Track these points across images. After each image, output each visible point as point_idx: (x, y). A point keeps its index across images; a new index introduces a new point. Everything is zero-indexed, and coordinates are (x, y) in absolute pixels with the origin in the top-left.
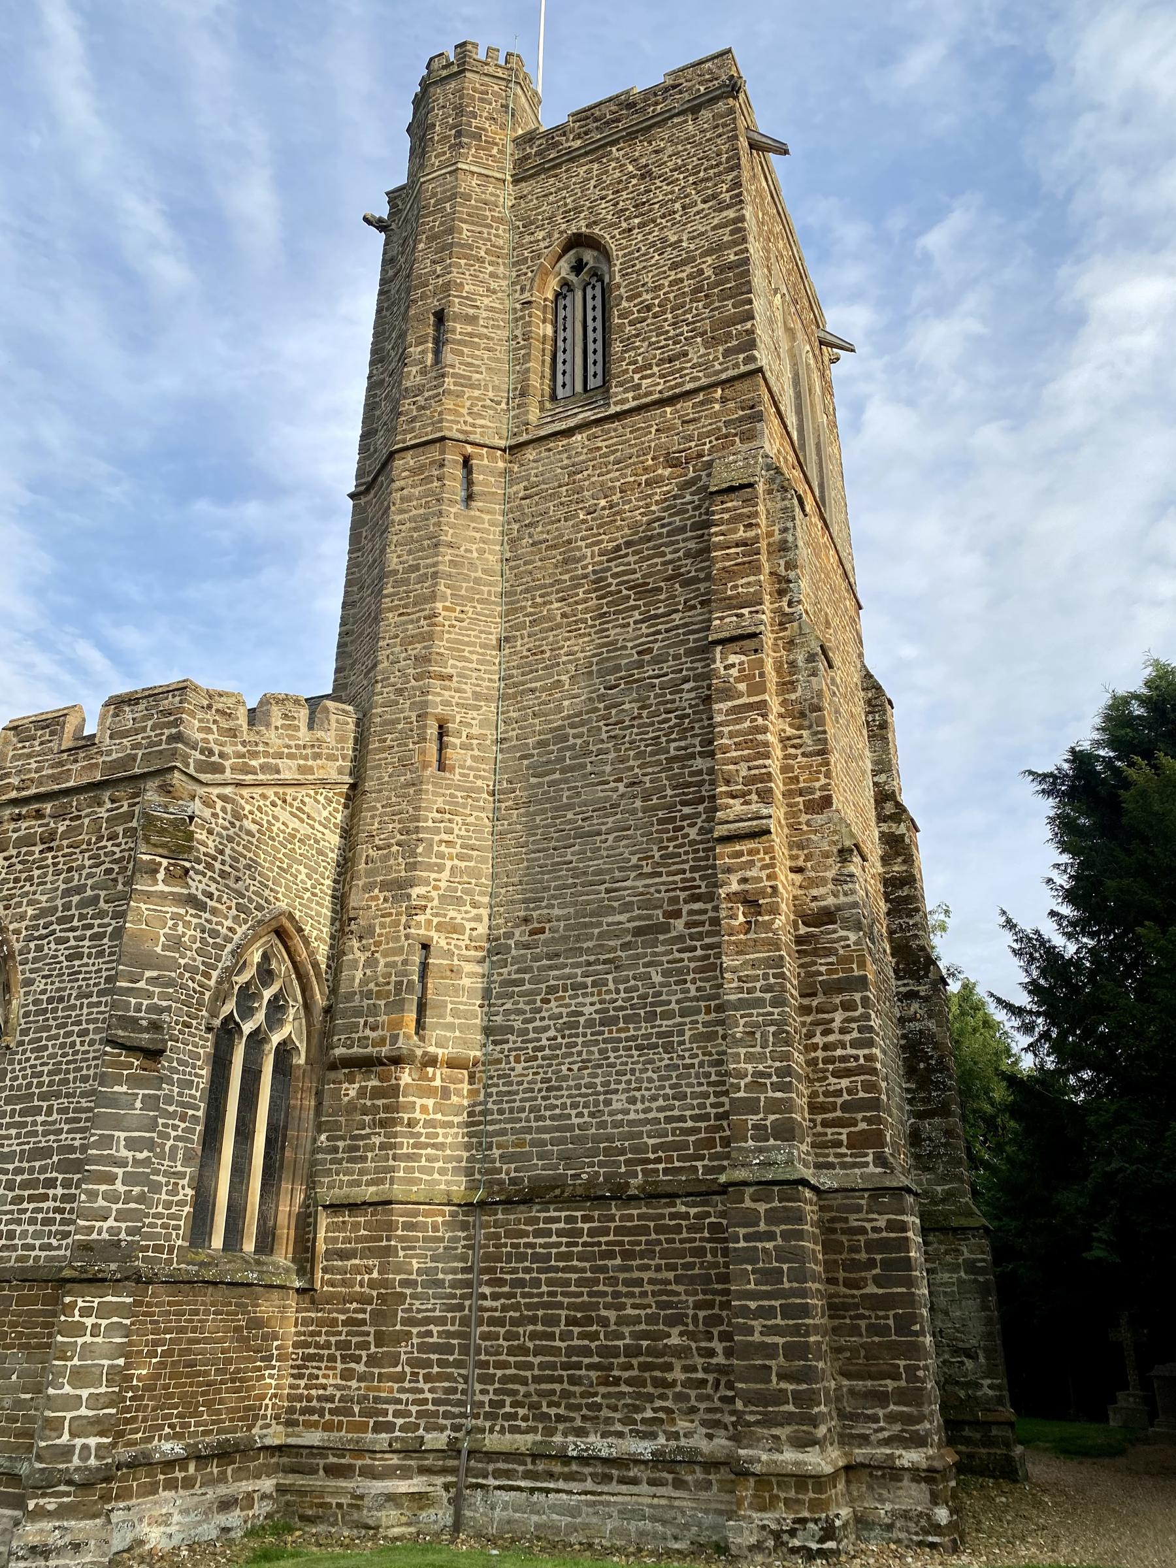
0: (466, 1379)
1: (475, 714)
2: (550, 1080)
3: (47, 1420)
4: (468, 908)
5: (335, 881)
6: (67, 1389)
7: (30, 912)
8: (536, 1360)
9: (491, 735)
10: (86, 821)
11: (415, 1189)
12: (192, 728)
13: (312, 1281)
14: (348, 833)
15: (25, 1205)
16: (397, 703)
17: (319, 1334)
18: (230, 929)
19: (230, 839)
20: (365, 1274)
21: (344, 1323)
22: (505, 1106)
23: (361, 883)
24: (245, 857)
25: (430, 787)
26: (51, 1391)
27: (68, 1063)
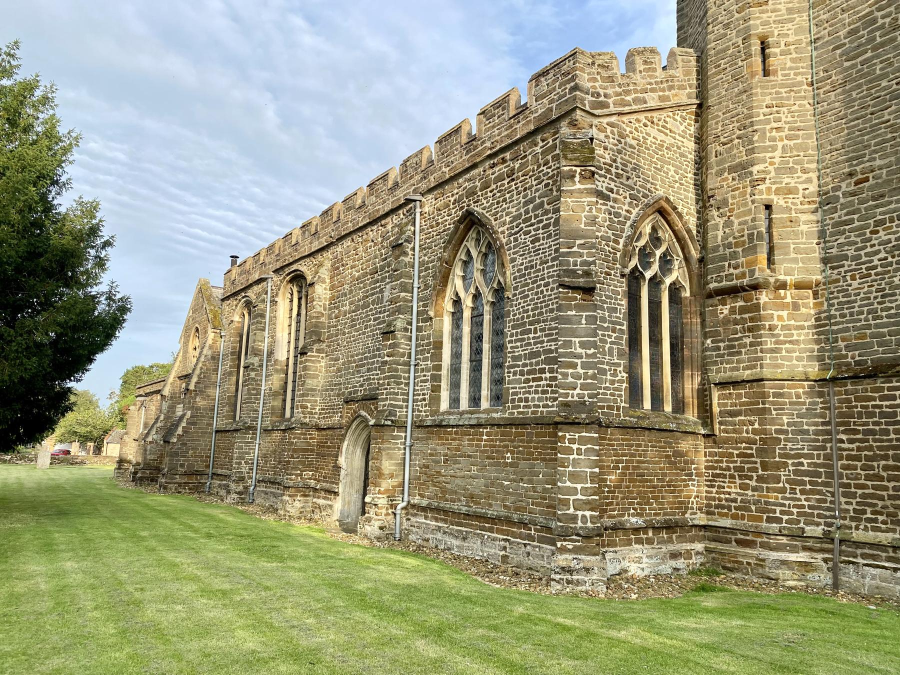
0: (833, 495)
1: (790, 25)
2: (884, 289)
3: (560, 499)
4: (799, 174)
5: (695, 174)
6: (568, 484)
7: (508, 219)
8: (891, 484)
9: (805, 38)
10: (530, 157)
11: (779, 371)
12: (584, 80)
13: (713, 429)
14: (700, 140)
15: (531, 383)
16: (726, 35)
17: (722, 462)
18: (628, 211)
19: (619, 152)
20: (749, 427)
21: (738, 456)
22: (846, 311)
23: (713, 171)
24: (631, 163)
25: (759, 90)
26: (559, 484)
27: (541, 303)
